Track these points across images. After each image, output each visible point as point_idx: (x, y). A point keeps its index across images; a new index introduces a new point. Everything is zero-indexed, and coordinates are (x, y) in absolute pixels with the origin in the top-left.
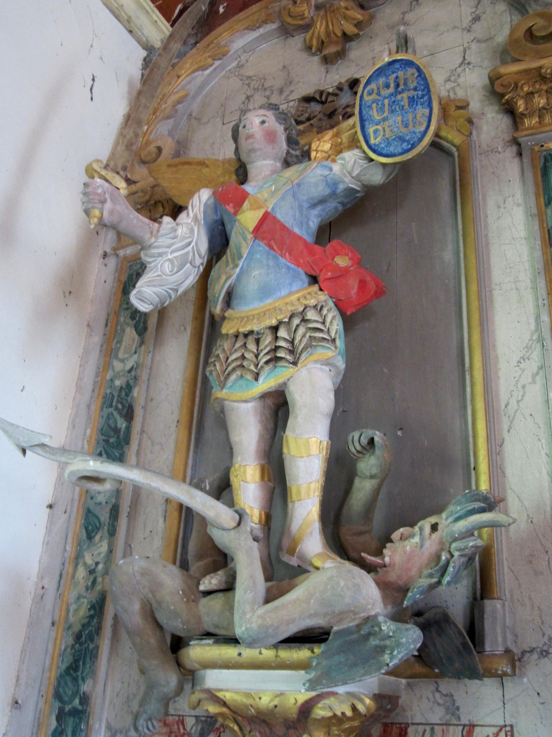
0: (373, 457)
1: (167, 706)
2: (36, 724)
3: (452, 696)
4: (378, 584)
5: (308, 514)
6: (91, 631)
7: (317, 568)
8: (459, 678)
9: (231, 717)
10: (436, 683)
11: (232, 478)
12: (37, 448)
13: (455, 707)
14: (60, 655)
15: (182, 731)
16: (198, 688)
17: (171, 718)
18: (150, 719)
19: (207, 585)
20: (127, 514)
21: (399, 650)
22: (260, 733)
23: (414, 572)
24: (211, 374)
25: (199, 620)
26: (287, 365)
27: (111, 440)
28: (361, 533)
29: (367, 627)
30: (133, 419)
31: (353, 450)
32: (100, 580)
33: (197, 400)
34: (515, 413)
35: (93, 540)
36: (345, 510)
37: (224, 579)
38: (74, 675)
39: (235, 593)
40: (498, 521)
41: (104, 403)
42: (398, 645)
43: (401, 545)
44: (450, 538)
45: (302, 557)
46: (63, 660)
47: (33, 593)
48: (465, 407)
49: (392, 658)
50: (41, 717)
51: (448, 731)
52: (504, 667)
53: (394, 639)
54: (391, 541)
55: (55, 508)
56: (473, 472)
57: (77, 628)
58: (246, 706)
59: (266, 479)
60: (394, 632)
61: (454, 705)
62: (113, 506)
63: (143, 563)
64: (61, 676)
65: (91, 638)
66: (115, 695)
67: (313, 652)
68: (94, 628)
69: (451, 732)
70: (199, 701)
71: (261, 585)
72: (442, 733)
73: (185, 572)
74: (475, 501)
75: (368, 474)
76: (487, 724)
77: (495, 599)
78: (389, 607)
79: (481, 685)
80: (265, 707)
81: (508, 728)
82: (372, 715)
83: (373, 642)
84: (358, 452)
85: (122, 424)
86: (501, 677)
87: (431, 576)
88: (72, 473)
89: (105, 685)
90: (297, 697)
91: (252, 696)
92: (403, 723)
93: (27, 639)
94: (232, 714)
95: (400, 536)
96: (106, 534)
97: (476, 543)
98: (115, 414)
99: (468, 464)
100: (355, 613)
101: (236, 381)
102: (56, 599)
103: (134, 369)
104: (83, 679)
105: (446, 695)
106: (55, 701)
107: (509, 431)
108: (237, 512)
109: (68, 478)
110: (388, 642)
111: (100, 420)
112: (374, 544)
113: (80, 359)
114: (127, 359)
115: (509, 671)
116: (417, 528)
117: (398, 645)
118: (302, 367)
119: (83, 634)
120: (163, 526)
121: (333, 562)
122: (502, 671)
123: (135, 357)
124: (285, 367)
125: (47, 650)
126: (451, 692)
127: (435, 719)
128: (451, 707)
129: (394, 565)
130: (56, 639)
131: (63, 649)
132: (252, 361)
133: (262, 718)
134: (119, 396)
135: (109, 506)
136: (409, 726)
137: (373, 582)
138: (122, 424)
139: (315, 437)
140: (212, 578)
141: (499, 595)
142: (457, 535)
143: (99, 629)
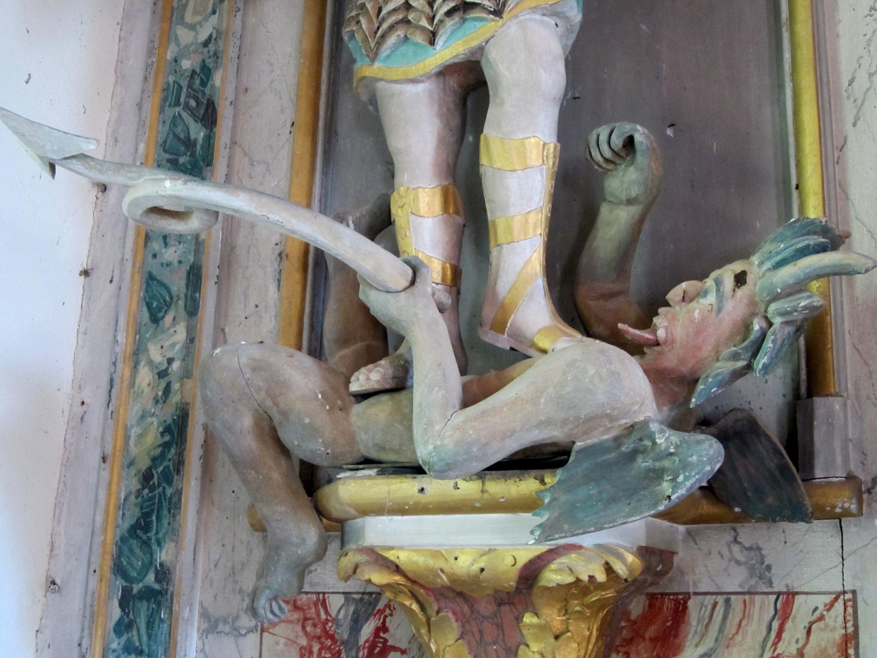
0: (632, 168)
1: (301, 577)
2: (88, 614)
3: (759, 549)
4: (647, 372)
5: (526, 264)
6: (168, 467)
7: (544, 352)
8: (774, 521)
9: (405, 590)
10: (734, 530)
11: (394, 210)
12: (74, 161)
13: (764, 565)
14: (119, 508)
15: (323, 616)
16: (353, 546)
17: (304, 597)
18: (275, 598)
19: (364, 383)
20: (216, 280)
21: (687, 474)
22: (454, 613)
23: (707, 351)
24: (352, 36)
25: (352, 440)
26: (485, 15)
27: (182, 160)
28: (612, 295)
29: (632, 440)
30: (216, 122)
31: (598, 157)
32: (176, 386)
33: (324, 87)
34: (865, 94)
35: (161, 322)
36: (584, 258)
37: (390, 372)
38: (144, 538)
39: (412, 393)
40: (848, 265)
41: (165, 100)
42: (685, 466)
43: (684, 310)
44: (768, 295)
45: (516, 335)
46: (124, 514)
47: (66, 413)
48: (781, 86)
49: (675, 487)
50: (95, 603)
51: (752, 602)
52: (845, 501)
53: (677, 459)
54: (667, 304)
55: (94, 276)
56: (795, 193)
57: (144, 464)
58: (434, 573)
59: (451, 211)
60: (677, 447)
61: (763, 563)
62: (192, 267)
63: (256, 352)
64: (123, 539)
65: (167, 477)
66: (212, 566)
67: (542, 482)
68: (171, 463)
69: (757, 604)
70: (356, 567)
71: (455, 380)
72: (743, 606)
73: (323, 365)
74: (808, 233)
75: (624, 197)
76: (815, 590)
77: (832, 395)
78: (665, 409)
79: (807, 531)
80: (465, 570)
81: (849, 596)
82: (635, 581)
83: (642, 463)
84: (607, 160)
85: (198, 132)
86: (839, 517)
87: (735, 357)
88: (135, 203)
89: (195, 550)
90: (516, 554)
91: (442, 555)
92: (681, 594)
93: (62, 484)
94: (409, 584)
95: (682, 295)
96: (182, 313)
97: (812, 302)
98: (185, 115)
99: (786, 181)
100: (612, 418)
101: (396, 47)
102: (106, 419)
103: (213, 40)
104: (159, 544)
105: (750, 549)
106: (116, 579)
107: (854, 125)
108: (408, 262)
109: (129, 211)
110: (666, 463)
111: (161, 127)
112: (633, 311)
113: (119, 26)
114: (200, 23)
115: (853, 507)
116: (709, 282)
117: (685, 466)
118: (510, 19)
119: (154, 472)
120: (276, 295)
121: (572, 341)
122: (842, 508)
123: (214, 19)
124: (481, 19)
125: (96, 501)
126: (757, 544)
127: (731, 585)
128: (757, 566)
129: (673, 341)
130: (110, 483)
131: (123, 498)
132: (422, 12)
133: (458, 589)
134: (190, 86)
135: (185, 268)
136: (690, 598)
137: (641, 369)
138: (198, 133)
139: (534, 137)
140: (370, 371)
141: (837, 390)
142: (779, 291)
143: (180, 464)
